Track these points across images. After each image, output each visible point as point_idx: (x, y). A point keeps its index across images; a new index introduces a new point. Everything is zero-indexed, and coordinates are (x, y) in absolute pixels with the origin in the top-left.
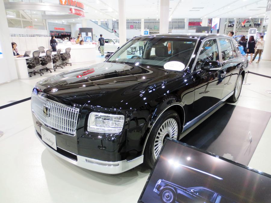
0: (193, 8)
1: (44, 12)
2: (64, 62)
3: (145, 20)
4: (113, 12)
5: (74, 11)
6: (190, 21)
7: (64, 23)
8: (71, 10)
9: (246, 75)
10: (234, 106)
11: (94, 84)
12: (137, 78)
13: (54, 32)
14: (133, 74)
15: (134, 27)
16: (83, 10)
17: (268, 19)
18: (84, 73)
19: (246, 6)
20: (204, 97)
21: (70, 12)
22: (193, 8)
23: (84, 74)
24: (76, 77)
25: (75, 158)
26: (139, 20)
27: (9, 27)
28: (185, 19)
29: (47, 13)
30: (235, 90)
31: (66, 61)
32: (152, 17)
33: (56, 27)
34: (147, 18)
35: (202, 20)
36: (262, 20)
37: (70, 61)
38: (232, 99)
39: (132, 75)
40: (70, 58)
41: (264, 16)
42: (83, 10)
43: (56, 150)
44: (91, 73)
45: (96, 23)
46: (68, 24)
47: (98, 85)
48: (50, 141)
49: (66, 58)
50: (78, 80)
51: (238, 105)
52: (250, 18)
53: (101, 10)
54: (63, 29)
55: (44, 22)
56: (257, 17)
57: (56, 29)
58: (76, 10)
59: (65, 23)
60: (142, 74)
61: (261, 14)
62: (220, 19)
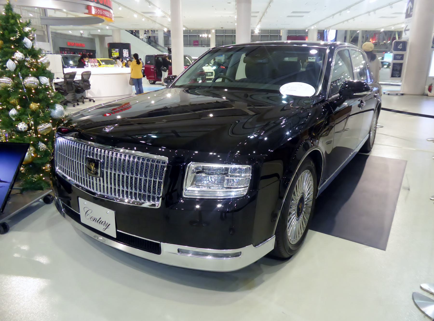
0: (294, 12)
1: (44, 10)
2: (79, 96)
3: (217, 31)
4: (164, 17)
5: (94, 11)
6: (290, 35)
7: (83, 36)
8: (89, 8)
9: (382, 111)
10: (368, 156)
11: (132, 123)
12: (201, 116)
13: (66, 49)
14: (195, 111)
15: (200, 43)
16: (111, 11)
17: (408, 30)
18: (113, 110)
19: (374, 10)
20: (336, 147)
21: (87, 11)
22: (294, 12)
23: (114, 111)
24: (101, 116)
25: (157, 250)
26: (278, 31)
27: (147, 56)
28: (281, 31)
29: (50, 14)
30: (370, 133)
31: (83, 94)
32: (228, 26)
33: (69, 41)
34: (219, 28)
35: (307, 33)
36: (400, 33)
37: (88, 94)
38: (367, 148)
39: (193, 113)
40: (89, 88)
41: (403, 28)
42: (111, 11)
43: (115, 236)
44: (125, 109)
45: (135, 33)
46: (90, 37)
47: (139, 124)
48: (101, 223)
49: (82, 88)
50: (105, 119)
51: (376, 155)
52: (382, 30)
53: (144, 13)
54: (81, 45)
55: (45, 29)
56: (393, 28)
57: (70, 44)
58: (97, 8)
59: (86, 35)
60: (209, 110)
61: (398, 24)
62: (337, 31)
